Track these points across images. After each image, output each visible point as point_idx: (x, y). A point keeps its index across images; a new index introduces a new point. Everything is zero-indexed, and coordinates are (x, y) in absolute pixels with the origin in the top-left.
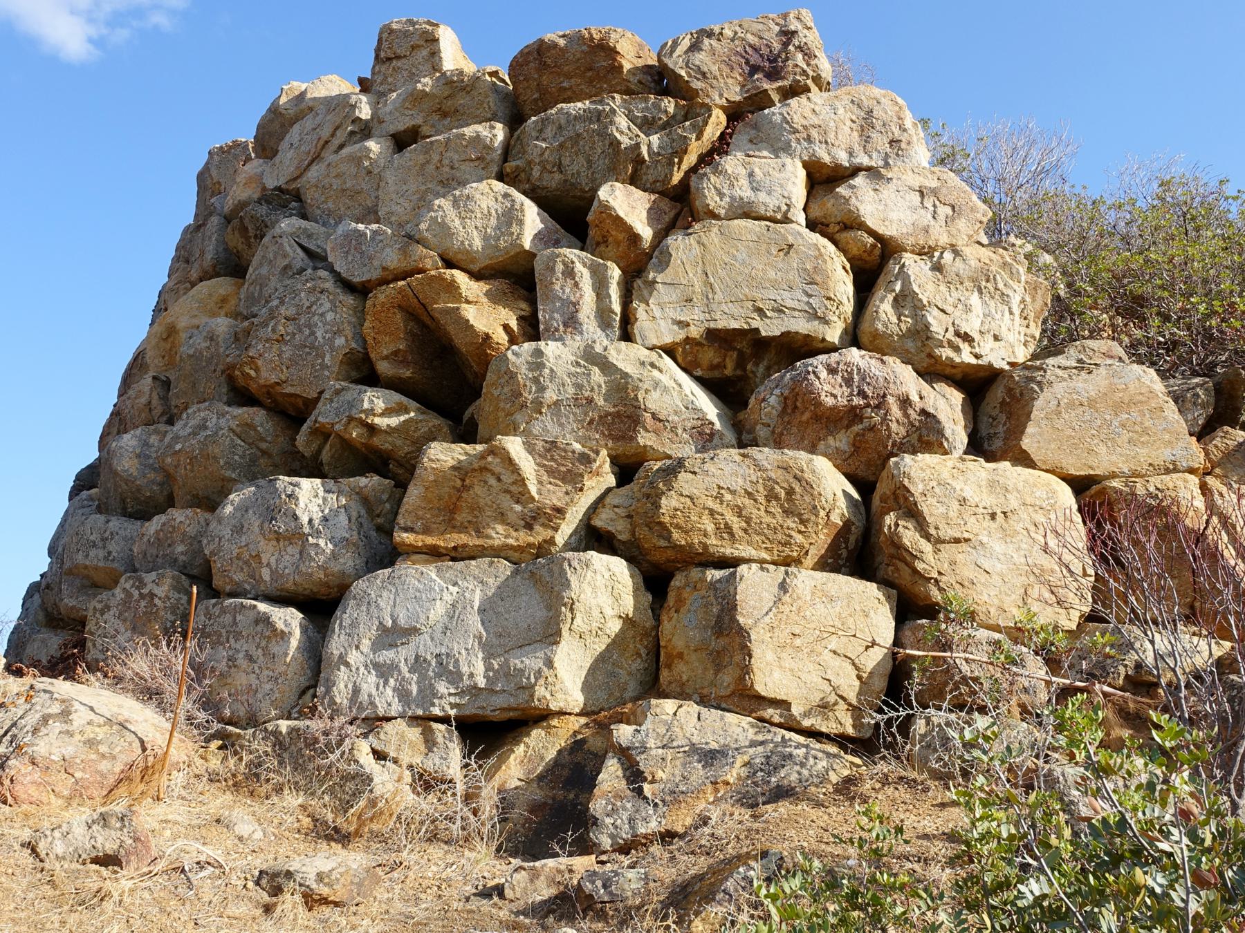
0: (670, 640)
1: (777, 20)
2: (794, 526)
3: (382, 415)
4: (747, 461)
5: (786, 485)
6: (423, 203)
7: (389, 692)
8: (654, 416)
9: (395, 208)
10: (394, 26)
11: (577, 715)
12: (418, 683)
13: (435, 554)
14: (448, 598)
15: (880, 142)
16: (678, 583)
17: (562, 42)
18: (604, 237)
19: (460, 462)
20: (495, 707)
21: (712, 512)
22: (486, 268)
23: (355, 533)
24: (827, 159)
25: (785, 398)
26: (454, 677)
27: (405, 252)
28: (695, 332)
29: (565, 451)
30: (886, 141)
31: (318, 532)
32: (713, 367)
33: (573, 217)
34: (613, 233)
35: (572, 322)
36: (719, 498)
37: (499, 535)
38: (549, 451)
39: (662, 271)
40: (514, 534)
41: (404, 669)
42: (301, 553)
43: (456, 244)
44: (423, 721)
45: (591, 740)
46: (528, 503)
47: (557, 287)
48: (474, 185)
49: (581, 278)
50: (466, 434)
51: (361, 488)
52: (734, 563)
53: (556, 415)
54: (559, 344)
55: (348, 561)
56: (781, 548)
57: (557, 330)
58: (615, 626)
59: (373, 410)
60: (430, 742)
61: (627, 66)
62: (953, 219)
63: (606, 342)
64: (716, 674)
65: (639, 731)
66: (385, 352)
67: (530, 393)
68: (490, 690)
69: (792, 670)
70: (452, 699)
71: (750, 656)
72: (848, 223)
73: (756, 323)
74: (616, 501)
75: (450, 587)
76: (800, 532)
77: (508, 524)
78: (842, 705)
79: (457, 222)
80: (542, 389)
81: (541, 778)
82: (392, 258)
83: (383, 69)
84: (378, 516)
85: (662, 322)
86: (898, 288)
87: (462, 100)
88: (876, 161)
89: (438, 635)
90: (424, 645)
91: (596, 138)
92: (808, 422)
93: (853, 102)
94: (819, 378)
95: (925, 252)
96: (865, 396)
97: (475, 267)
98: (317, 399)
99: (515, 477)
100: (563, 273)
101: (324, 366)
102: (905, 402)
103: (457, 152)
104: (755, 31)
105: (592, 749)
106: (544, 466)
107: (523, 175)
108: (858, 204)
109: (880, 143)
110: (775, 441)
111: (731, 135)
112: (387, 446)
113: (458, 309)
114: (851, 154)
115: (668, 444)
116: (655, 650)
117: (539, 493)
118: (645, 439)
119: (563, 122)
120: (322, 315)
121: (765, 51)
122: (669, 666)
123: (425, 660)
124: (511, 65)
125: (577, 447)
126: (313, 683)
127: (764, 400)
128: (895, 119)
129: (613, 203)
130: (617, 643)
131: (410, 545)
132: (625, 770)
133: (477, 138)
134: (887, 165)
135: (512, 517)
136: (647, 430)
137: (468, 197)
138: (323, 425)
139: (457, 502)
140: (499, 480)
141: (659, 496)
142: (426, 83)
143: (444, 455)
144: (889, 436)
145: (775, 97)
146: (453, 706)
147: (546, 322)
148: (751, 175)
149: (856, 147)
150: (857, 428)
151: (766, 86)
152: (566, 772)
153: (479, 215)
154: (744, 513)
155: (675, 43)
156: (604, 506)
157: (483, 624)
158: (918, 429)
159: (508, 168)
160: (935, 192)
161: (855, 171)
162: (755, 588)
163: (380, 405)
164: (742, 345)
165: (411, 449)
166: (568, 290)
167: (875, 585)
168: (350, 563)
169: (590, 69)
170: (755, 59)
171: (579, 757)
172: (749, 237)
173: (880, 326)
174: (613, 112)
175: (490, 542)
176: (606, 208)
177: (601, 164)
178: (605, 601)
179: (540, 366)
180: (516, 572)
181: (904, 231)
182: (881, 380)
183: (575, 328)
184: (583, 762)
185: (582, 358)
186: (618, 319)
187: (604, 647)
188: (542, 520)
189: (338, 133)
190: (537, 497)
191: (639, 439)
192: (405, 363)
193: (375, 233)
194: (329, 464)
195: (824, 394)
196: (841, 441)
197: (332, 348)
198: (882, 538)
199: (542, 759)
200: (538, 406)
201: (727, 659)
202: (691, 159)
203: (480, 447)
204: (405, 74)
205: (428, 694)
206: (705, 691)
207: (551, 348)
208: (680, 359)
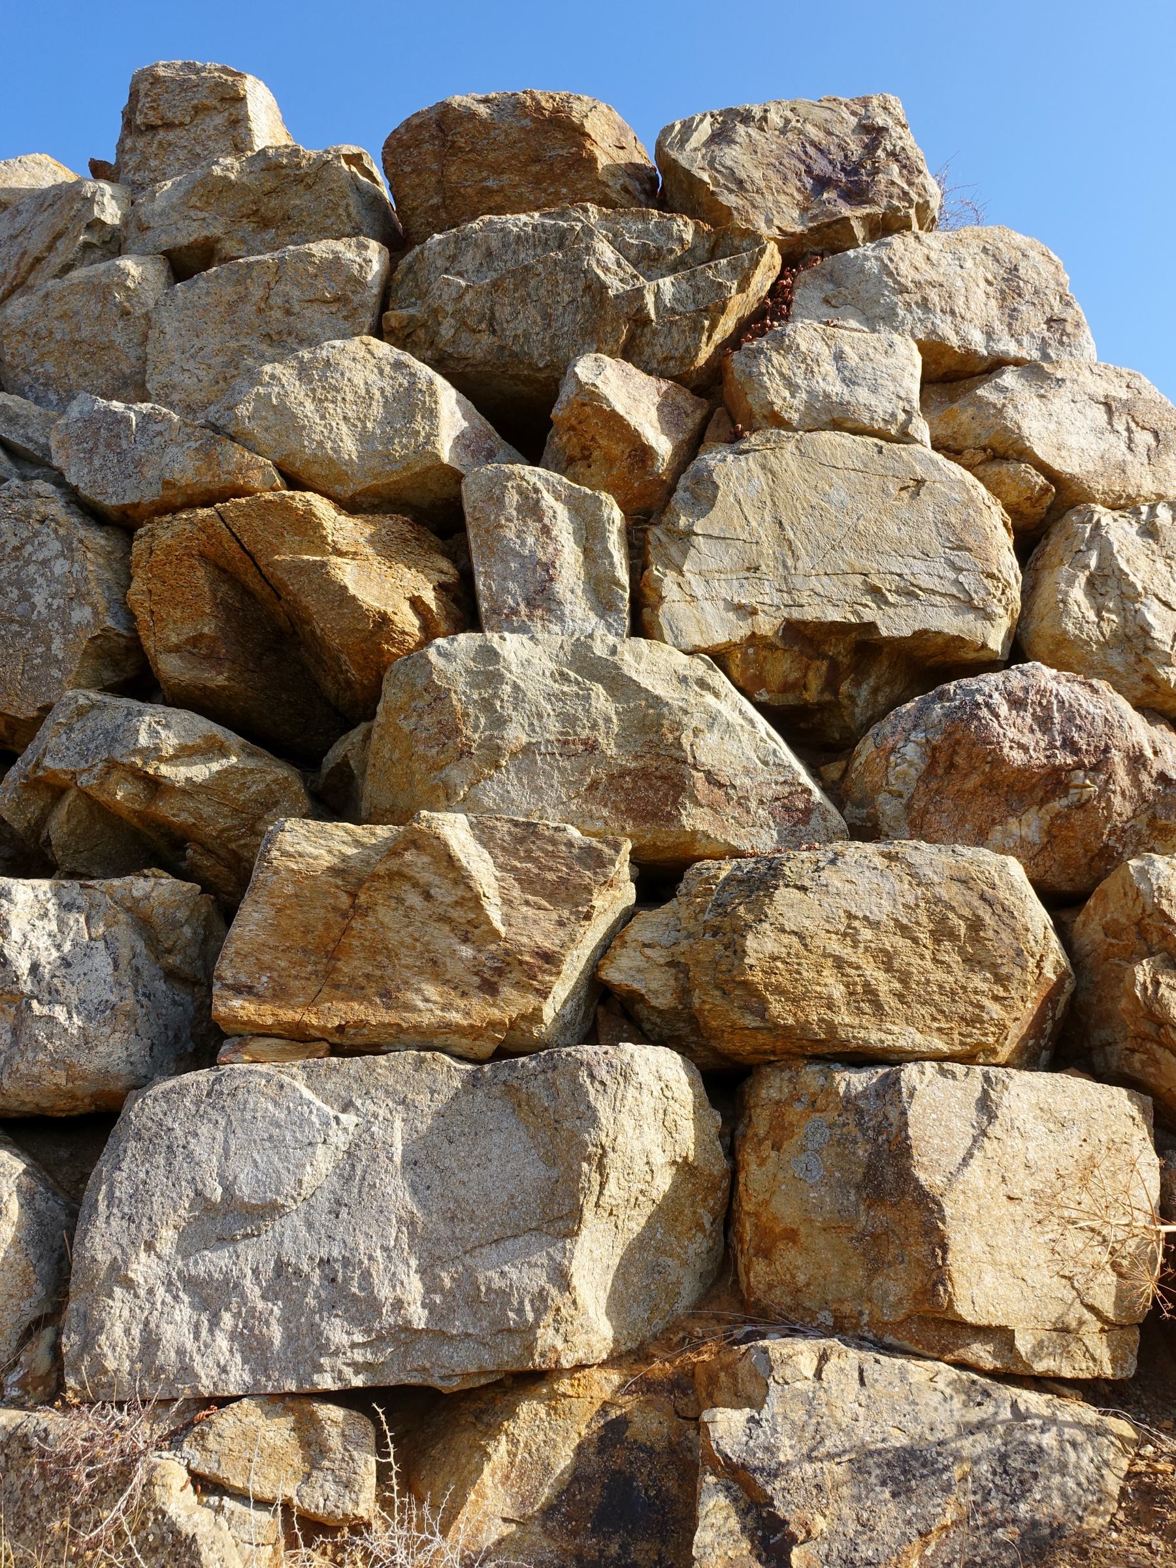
0: (766, 1203)
1: (855, 107)
2: (984, 987)
3: (170, 760)
4: (897, 868)
5: (967, 912)
6: (234, 372)
7: (222, 1342)
8: (711, 778)
9: (177, 377)
10: (161, 72)
11: (602, 1365)
12: (284, 1321)
13: (298, 1039)
14: (340, 1140)
15: (1033, 319)
16: (775, 1094)
17: (483, 110)
18: (584, 448)
19: (345, 858)
20: (456, 1365)
21: (840, 963)
22: (365, 492)
23: (128, 992)
24: (954, 341)
25: (934, 749)
26: (362, 1310)
27: (208, 455)
28: (767, 625)
29: (554, 842)
30: (1041, 319)
31: (53, 992)
32: (786, 688)
33: (524, 413)
34: (603, 442)
35: (542, 598)
36: (849, 935)
37: (429, 1003)
38: (520, 843)
39: (703, 514)
40: (461, 1003)
41: (253, 1292)
42: (15, 1031)
43: (309, 447)
44: (297, 1403)
45: (637, 1419)
46: (486, 942)
47: (510, 533)
48: (338, 343)
49: (550, 521)
50: (334, 800)
51: (136, 901)
52: (892, 1058)
53: (528, 772)
54: (524, 638)
55: (114, 1052)
56: (965, 1030)
57: (515, 612)
58: (664, 1182)
59: (157, 749)
60: (313, 1447)
61: (603, 161)
62: (1159, 455)
63: (611, 639)
64: (870, 1279)
65: (758, 1423)
66: (174, 639)
67: (476, 728)
68: (437, 1335)
69: (1011, 1267)
70: (358, 1356)
71: (945, 1248)
72: (1001, 450)
73: (870, 614)
74: (647, 936)
75: (343, 1117)
76: (996, 998)
77: (446, 982)
78: (1094, 1325)
79: (310, 407)
80: (499, 722)
81: (549, 1511)
82: (183, 466)
83: (140, 144)
84: (169, 951)
85: (707, 605)
86: (1093, 563)
87: (298, 200)
88: (1029, 352)
89: (322, 1218)
90: (293, 1238)
91: (561, 276)
92: (970, 789)
93: (985, 250)
94: (997, 716)
95: (1124, 504)
96: (1074, 748)
97: (346, 491)
98: (36, 723)
99: (460, 892)
100: (519, 509)
101: (49, 660)
102: (1136, 761)
103: (297, 284)
104: (819, 121)
105: (642, 1438)
106: (514, 869)
107: (421, 333)
108: (1017, 417)
109: (1034, 321)
110: (912, 824)
111: (791, 289)
112: (185, 818)
113: (324, 565)
114: (989, 335)
115: (733, 828)
116: (728, 1219)
117: (507, 922)
118: (694, 818)
119: (495, 245)
120: (45, 563)
121: (838, 156)
122: (766, 1253)
123: (298, 1273)
124: (387, 145)
125: (574, 833)
126: (48, 1309)
127: (893, 750)
128: (1052, 284)
129: (604, 389)
130: (667, 1213)
131: (249, 1022)
132: (743, 1513)
133: (335, 264)
134: (1046, 357)
135: (454, 970)
136: (698, 804)
137: (328, 363)
138: (54, 774)
139: (339, 931)
140: (428, 896)
141: (742, 930)
142: (228, 166)
143: (308, 846)
144: (1108, 819)
145: (859, 232)
146: (358, 1368)
147: (492, 597)
148: (839, 357)
149: (997, 325)
150: (1059, 804)
151: (846, 211)
152: (595, 1494)
153: (350, 397)
154: (896, 965)
155: (688, 128)
156: (624, 944)
157: (415, 1191)
158: (1152, 805)
159: (390, 315)
160: (1128, 408)
161: (997, 364)
162: (937, 1105)
163: (170, 741)
164: (837, 649)
165: (230, 822)
166: (530, 540)
167: (1124, 1092)
168: (120, 1053)
169: (537, 160)
170: (821, 166)
171: (618, 1459)
172: (849, 464)
173: (1070, 627)
174: (589, 232)
175: (413, 1018)
176: (591, 398)
177: (567, 321)
178: (653, 1137)
179: (495, 679)
180: (473, 1082)
181: (1091, 467)
182: (1099, 722)
183: (550, 610)
184: (627, 1469)
185: (570, 665)
186: (627, 596)
187: (643, 1222)
188: (516, 975)
189: (61, 245)
190: (503, 930)
191: (684, 820)
192: (212, 659)
193: (146, 418)
194: (64, 847)
195: (1007, 744)
196: (1029, 826)
197: (66, 626)
198: (1124, 1004)
199: (547, 1468)
200: (493, 754)
201: (894, 1250)
202: (727, 325)
203: (383, 832)
204: (182, 154)
205: (308, 1346)
206: (846, 1308)
207: (512, 647)
208: (736, 673)
